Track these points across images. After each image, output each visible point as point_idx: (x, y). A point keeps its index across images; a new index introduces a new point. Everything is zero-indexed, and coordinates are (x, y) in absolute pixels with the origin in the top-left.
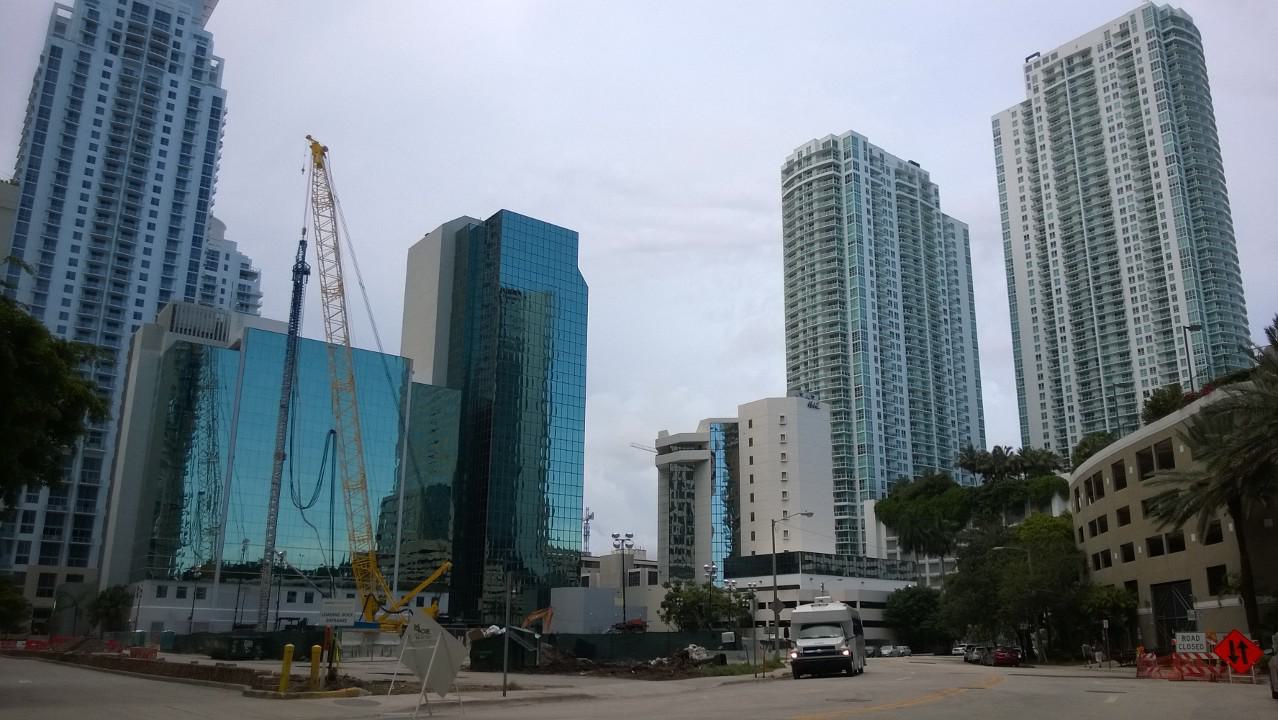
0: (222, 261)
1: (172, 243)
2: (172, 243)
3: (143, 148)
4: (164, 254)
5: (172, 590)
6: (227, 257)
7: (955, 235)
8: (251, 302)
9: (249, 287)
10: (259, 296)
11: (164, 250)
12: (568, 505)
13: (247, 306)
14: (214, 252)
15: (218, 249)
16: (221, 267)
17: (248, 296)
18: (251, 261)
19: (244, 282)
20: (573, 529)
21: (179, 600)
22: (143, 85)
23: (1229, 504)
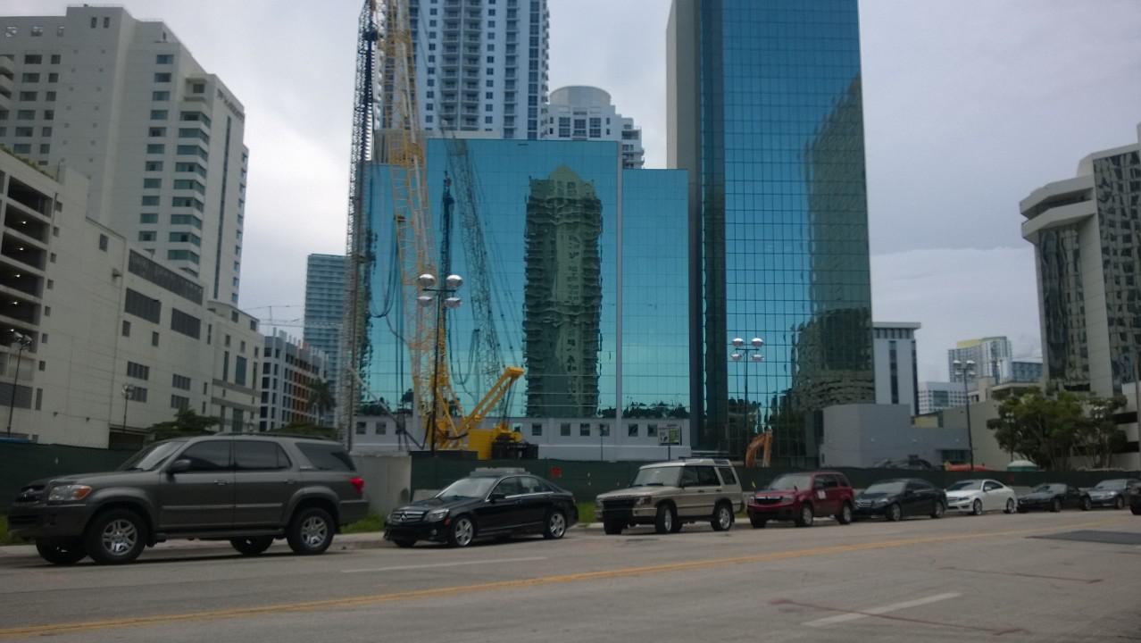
0: (604, 127)
1: (511, 23)
2: (511, 23)
3: (450, 35)
4: (503, 119)
5: (391, 426)
6: (608, 121)
7: (693, 522)
8: (635, 159)
9: (632, 146)
10: (642, 153)
11: (505, 42)
12: (740, 266)
13: (632, 165)
14: (596, 119)
15: (598, 116)
16: (603, 132)
17: (632, 155)
18: (631, 120)
19: (627, 142)
20: (740, 266)
21: (564, 437)
22: (464, 46)
23: (727, 399)
